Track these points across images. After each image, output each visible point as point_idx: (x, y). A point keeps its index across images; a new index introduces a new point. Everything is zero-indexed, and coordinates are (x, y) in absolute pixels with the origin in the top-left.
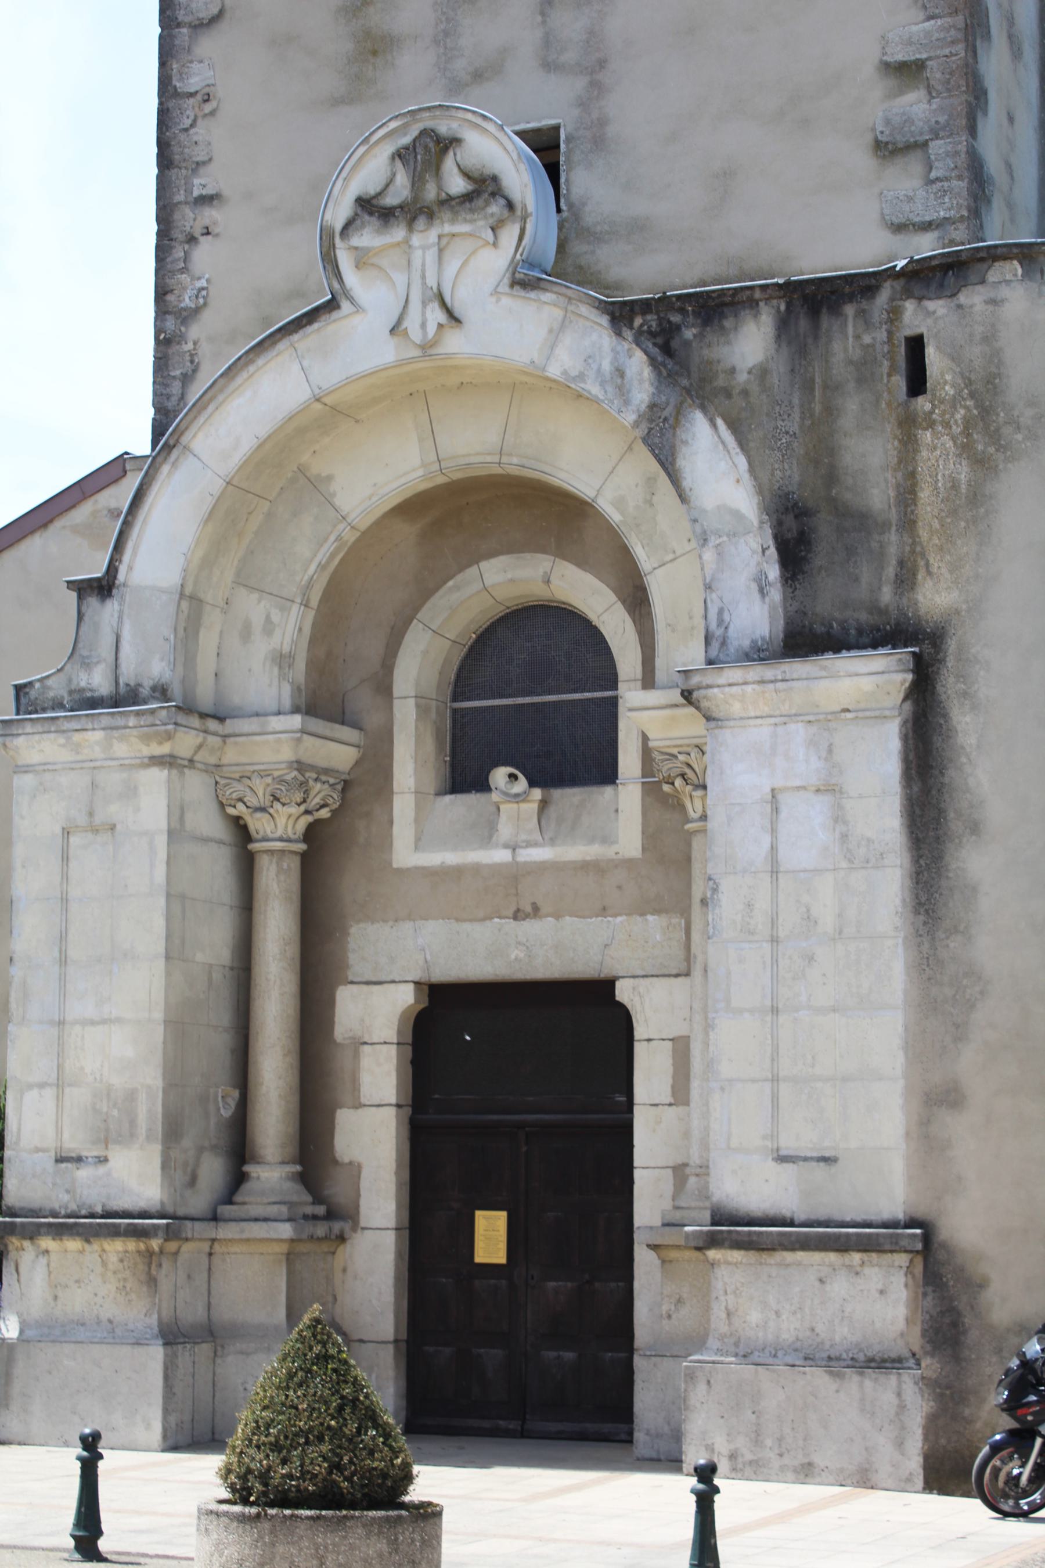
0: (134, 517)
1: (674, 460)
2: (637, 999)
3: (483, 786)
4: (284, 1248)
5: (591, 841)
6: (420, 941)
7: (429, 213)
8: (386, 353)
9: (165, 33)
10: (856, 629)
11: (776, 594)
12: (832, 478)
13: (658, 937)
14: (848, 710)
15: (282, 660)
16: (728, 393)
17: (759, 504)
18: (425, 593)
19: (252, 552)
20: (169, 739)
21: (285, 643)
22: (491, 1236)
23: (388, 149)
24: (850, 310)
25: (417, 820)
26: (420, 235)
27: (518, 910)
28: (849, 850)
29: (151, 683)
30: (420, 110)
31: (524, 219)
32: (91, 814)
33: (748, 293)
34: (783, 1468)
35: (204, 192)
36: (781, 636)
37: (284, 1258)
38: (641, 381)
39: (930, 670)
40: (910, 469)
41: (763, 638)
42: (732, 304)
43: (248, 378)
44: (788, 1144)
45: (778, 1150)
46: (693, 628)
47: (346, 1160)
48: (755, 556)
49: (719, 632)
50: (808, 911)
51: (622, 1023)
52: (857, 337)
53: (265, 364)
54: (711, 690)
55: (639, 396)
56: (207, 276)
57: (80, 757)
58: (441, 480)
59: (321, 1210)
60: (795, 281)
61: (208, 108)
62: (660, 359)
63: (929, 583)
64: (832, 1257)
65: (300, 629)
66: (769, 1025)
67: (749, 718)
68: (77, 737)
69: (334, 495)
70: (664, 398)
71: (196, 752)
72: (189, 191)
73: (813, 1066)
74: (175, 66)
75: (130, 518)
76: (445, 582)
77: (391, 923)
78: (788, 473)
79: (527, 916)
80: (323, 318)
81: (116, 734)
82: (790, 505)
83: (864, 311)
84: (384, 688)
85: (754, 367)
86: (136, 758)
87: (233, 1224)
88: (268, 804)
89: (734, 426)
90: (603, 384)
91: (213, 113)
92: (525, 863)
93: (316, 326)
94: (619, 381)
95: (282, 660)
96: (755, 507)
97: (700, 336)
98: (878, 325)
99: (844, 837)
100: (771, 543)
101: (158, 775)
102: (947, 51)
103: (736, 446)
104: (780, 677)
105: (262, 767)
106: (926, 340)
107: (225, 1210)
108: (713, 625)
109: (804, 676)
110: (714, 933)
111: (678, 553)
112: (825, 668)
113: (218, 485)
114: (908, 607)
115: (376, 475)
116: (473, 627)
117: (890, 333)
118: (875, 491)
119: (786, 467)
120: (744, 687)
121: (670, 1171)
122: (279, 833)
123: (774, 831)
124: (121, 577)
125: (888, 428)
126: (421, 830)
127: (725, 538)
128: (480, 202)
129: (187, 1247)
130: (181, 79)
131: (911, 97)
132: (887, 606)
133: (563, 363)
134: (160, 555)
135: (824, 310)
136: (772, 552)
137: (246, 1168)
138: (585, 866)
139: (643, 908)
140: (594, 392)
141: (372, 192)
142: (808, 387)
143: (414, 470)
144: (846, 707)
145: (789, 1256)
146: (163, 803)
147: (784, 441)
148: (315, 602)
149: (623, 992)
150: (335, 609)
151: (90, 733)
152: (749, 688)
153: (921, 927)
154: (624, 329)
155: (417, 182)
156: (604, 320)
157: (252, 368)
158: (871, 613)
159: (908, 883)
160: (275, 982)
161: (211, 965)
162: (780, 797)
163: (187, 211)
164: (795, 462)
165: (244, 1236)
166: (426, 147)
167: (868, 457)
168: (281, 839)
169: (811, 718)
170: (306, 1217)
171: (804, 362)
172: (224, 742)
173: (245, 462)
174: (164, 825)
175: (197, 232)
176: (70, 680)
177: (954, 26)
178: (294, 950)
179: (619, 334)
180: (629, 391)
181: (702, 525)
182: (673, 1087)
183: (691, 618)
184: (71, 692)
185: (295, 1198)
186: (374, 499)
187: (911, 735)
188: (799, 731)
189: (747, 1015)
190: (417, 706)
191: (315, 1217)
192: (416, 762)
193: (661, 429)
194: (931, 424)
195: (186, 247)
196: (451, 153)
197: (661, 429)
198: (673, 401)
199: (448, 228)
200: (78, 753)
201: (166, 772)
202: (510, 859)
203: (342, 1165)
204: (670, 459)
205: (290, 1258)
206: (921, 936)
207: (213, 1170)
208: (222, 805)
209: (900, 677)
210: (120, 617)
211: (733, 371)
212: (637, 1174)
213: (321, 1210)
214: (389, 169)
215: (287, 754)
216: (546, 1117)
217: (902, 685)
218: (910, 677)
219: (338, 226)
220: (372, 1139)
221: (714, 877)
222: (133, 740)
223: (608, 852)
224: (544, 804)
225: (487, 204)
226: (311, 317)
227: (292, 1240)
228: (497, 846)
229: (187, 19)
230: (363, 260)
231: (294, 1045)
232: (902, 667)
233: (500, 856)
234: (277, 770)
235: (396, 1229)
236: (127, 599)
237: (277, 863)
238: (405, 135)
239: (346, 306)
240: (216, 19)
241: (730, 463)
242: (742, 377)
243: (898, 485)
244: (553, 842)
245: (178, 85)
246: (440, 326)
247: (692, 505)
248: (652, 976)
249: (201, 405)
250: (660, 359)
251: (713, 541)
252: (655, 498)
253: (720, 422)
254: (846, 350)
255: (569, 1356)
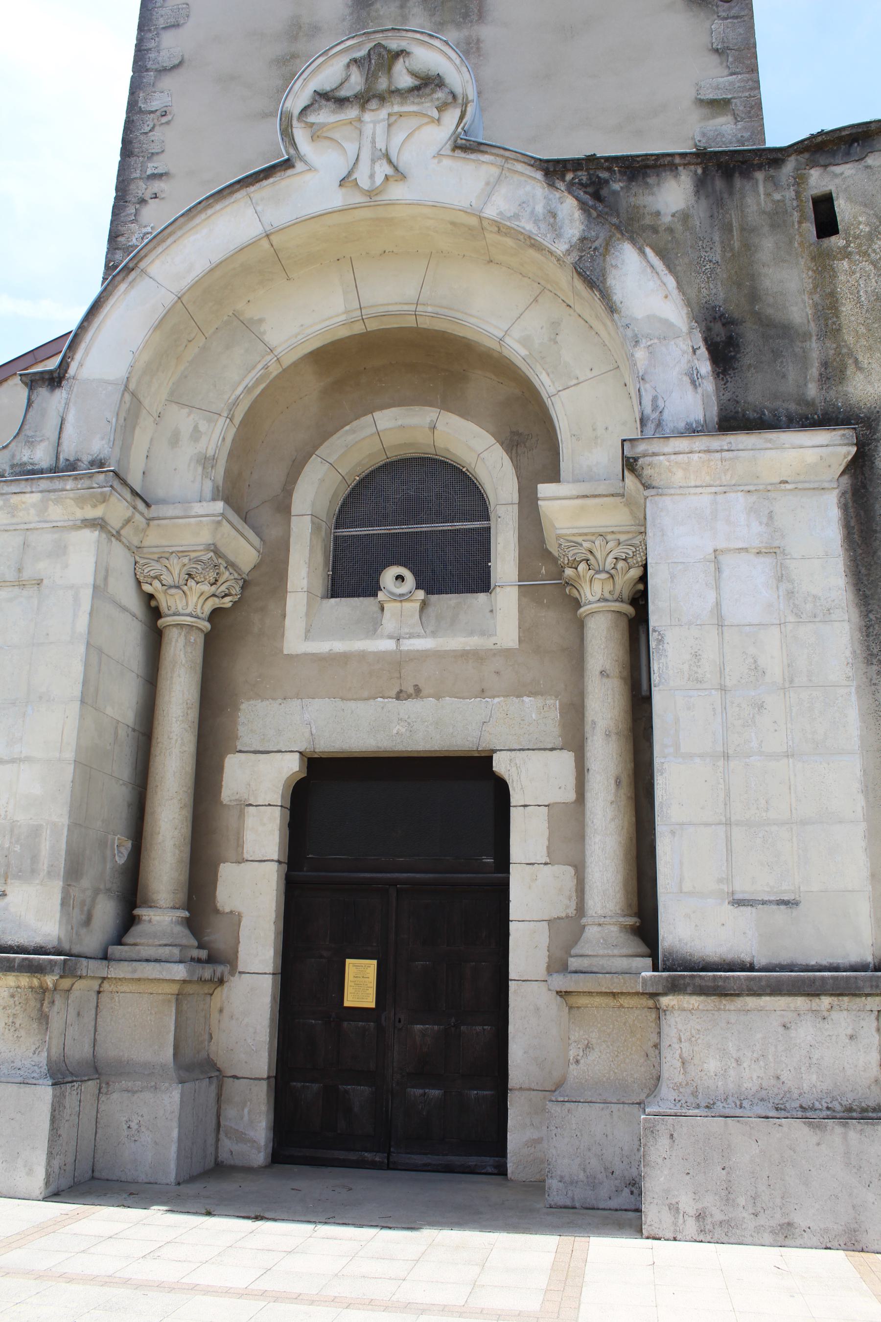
0: (90, 324)
1: (605, 279)
2: (514, 769)
3: (371, 589)
4: (175, 988)
5: (472, 633)
6: (307, 716)
7: (382, 98)
8: (337, 199)
9: (136, 75)
10: (786, 416)
11: (709, 385)
12: (754, 296)
13: (534, 716)
14: (787, 482)
15: (206, 462)
16: (655, 230)
17: (687, 314)
18: (324, 433)
19: (186, 377)
20: (104, 502)
21: (210, 448)
22: (360, 982)
23: (345, 59)
24: (760, 176)
25: (307, 614)
26: (372, 113)
27: (401, 691)
28: (795, 605)
29: (90, 458)
30: (375, 32)
31: (465, 104)
32: (20, 570)
33: (669, 159)
34: (758, 1229)
35: (156, 172)
36: (716, 419)
37: (173, 999)
38: (572, 221)
39: (867, 448)
40: (828, 290)
41: (697, 422)
42: (654, 167)
43: (205, 220)
44: (744, 887)
45: (733, 893)
46: (596, 438)
47: (227, 910)
48: (686, 355)
49: (655, 415)
50: (755, 662)
51: (501, 789)
52: (768, 195)
53: (222, 209)
54: (657, 458)
55: (571, 232)
56: (152, 225)
57: (14, 520)
58: (358, 329)
59: (203, 954)
60: (711, 152)
61: (164, 120)
62: (591, 203)
63: (860, 376)
64: (800, 1002)
65: (224, 439)
66: (721, 769)
67: (688, 487)
68: (15, 499)
69: (264, 333)
70: (593, 234)
71: (122, 528)
72: (144, 171)
73: (767, 810)
74: (141, 95)
75: (85, 324)
76: (342, 428)
77: (280, 701)
78: (714, 291)
79: (409, 696)
80: (279, 174)
81: (52, 496)
82: (717, 316)
83: (772, 177)
84: (283, 506)
85: (677, 212)
86: (69, 520)
87: (126, 963)
88: (182, 582)
89: (661, 253)
90: (536, 222)
91: (168, 123)
92: (408, 651)
93: (271, 180)
94: (552, 220)
95: (206, 462)
96: (685, 316)
97: (628, 188)
98: (785, 186)
99: (790, 594)
100: (701, 344)
101: (91, 536)
102: (747, 94)
103: (664, 269)
104: (726, 448)
105: (181, 549)
106: (834, 198)
107: (116, 950)
108: (648, 410)
109: (750, 447)
110: (660, 681)
111: (581, 379)
112: (770, 441)
113: (170, 299)
114: (837, 399)
115: (306, 317)
116: (359, 470)
117: (798, 194)
118: (794, 309)
119: (712, 286)
120: (689, 455)
121: (545, 924)
122: (188, 611)
123: (718, 588)
124: (71, 371)
125: (802, 262)
126: (308, 623)
127: (656, 341)
128: (428, 90)
129: (80, 985)
130: (145, 102)
131: (721, 120)
132: (813, 400)
133: (498, 206)
134: (101, 363)
135: (737, 175)
136: (703, 351)
137: (137, 912)
138: (464, 655)
139: (518, 691)
140: (527, 228)
141: (328, 89)
142: (727, 228)
143: (338, 316)
144: (785, 479)
145: (751, 1002)
146: (92, 560)
147: (708, 267)
148: (237, 420)
149: (501, 765)
150: (250, 433)
151: (28, 495)
152: (695, 457)
153: (875, 676)
154: (557, 181)
155: (370, 78)
156: (539, 175)
157: (210, 212)
158: (799, 404)
159: (858, 635)
160: (177, 740)
161: (118, 722)
162: (720, 558)
163: (141, 184)
164: (719, 283)
165: (136, 976)
166: (380, 55)
167: (787, 283)
168: (190, 615)
169: (751, 488)
170: (192, 959)
171: (721, 211)
172: (148, 525)
173: (197, 282)
174: (90, 580)
175: (147, 196)
176: (13, 456)
177: (751, 79)
178: (194, 714)
179: (552, 185)
180: (561, 228)
181: (634, 331)
182: (548, 847)
183: (594, 430)
184: (12, 466)
185: (184, 942)
186: (299, 337)
187: (850, 505)
188: (739, 501)
189: (697, 760)
190: (313, 523)
191: (199, 961)
192: (309, 567)
193: (592, 256)
194: (848, 255)
195: (137, 206)
196: (401, 60)
197: (592, 256)
198: (602, 236)
199: (397, 108)
200: (14, 516)
201: (97, 533)
202: (395, 648)
203: (223, 913)
204: (601, 279)
205: (179, 997)
206: (875, 684)
207: (106, 912)
208: (139, 583)
209: (844, 450)
210: (67, 404)
211: (658, 214)
212: (512, 926)
213: (203, 954)
214: (344, 73)
215: (205, 537)
216: (418, 876)
217: (845, 458)
218: (854, 450)
219: (296, 112)
220: (253, 891)
221: (659, 629)
222: (69, 502)
223: (487, 643)
224: (424, 604)
225: (433, 91)
226: (267, 173)
227: (184, 981)
228: (382, 637)
229: (154, 67)
230: (317, 134)
231: (188, 799)
232: (846, 441)
233: (386, 645)
234: (194, 551)
235: (273, 974)
236: (75, 389)
237: (185, 636)
238: (359, 51)
239: (299, 166)
240: (180, 64)
241: (659, 282)
242: (667, 219)
243: (815, 305)
244: (434, 634)
245: (142, 106)
246: (387, 178)
247: (623, 314)
248: (528, 749)
249: (160, 238)
250: (591, 203)
251: (644, 343)
252: (559, 338)
253: (648, 250)
254: (759, 204)
255: (435, 1093)
